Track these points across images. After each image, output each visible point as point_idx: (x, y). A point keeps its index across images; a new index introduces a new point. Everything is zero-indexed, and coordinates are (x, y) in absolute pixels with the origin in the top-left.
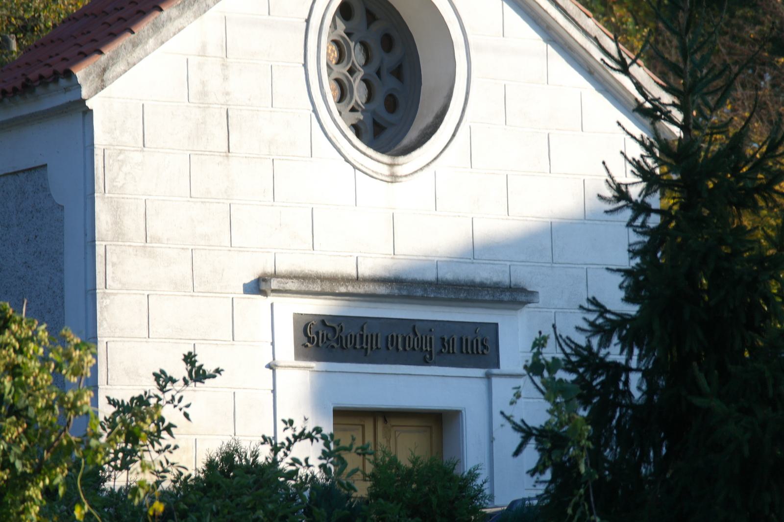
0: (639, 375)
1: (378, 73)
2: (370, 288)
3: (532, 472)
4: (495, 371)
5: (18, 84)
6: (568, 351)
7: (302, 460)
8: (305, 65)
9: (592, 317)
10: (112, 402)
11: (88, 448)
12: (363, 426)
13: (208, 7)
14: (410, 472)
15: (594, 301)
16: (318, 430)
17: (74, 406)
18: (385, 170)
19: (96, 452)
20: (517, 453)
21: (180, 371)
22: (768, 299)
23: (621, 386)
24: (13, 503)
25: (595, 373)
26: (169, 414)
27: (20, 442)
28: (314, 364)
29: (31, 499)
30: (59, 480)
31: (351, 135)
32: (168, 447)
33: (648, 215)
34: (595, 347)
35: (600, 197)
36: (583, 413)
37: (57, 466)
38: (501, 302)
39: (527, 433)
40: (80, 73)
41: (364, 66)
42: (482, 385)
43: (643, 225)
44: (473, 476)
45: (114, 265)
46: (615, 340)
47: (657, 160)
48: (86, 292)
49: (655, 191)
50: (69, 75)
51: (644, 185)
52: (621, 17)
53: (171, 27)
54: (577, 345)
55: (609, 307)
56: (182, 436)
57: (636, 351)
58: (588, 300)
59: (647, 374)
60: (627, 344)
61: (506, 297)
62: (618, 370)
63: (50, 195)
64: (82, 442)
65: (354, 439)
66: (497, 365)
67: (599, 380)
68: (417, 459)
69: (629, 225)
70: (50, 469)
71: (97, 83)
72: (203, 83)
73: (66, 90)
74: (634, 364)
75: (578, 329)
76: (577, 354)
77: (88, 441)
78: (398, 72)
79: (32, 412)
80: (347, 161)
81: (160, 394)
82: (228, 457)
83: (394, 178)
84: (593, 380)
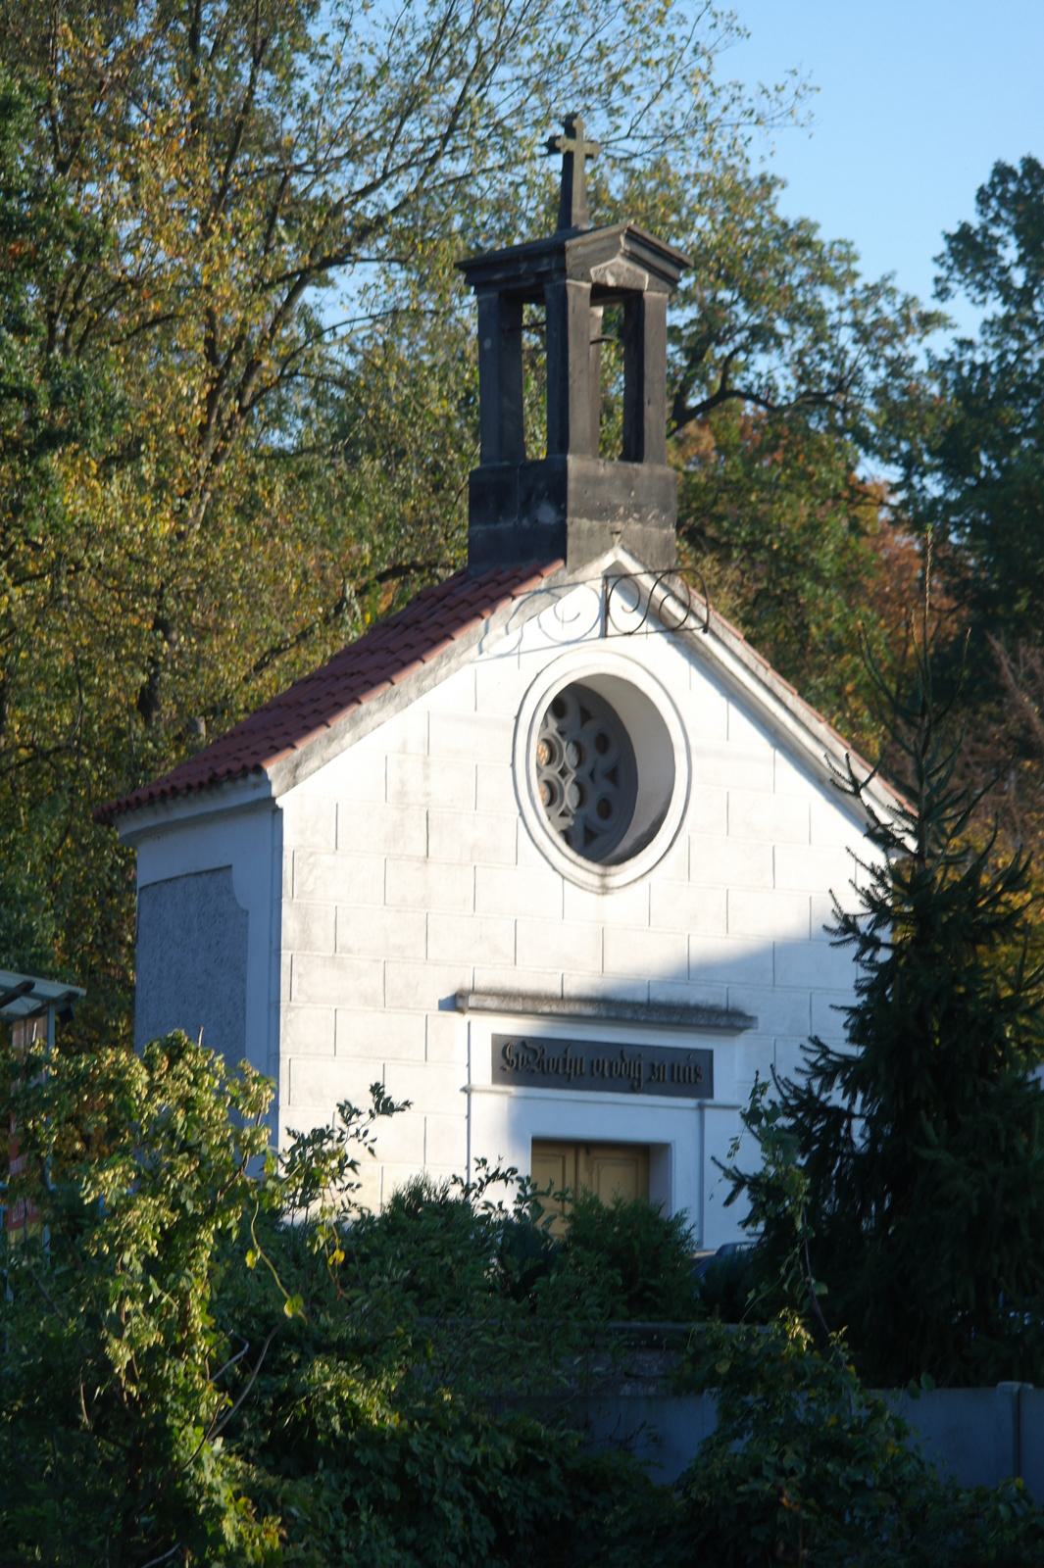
0: (862, 1122)
1: (592, 775)
2: (575, 1008)
3: (745, 1224)
4: (708, 1101)
5: (205, 778)
6: (786, 1093)
7: (496, 1205)
8: (513, 765)
9: (813, 1058)
10: (291, 1133)
11: (265, 1190)
12: (564, 1158)
13: (411, 701)
14: (611, 1215)
15: (815, 1041)
16: (513, 1171)
17: (250, 1144)
18: (595, 881)
19: (273, 1195)
20: (728, 1202)
21: (366, 1102)
22: (1003, 1043)
23: (843, 1133)
24: (183, 1247)
25: (815, 1119)
26: (353, 1149)
27: (192, 1181)
28: (512, 1089)
29: (202, 1242)
30: (232, 1223)
31: (560, 842)
32: (350, 1185)
33: (877, 949)
34: (816, 1090)
35: (826, 928)
36: (802, 1162)
37: (230, 1208)
38: (717, 1027)
39: (740, 1181)
40: (271, 769)
41: (576, 768)
42: (694, 1116)
43: (871, 959)
44: (680, 1220)
45: (300, 975)
46: (838, 1083)
47: (888, 890)
48: (270, 1005)
49: (886, 923)
50: (259, 770)
51: (873, 916)
52: (857, 710)
53: (369, 722)
54: (796, 1088)
55: (832, 1047)
56: (368, 1169)
57: (860, 1097)
58: (810, 1039)
59: (870, 1121)
60: (850, 1088)
61: (723, 1021)
62: (840, 1116)
63: (234, 899)
64: (257, 1184)
65: (552, 1183)
66: (711, 1095)
67: (819, 1126)
68: (620, 1200)
69: (856, 959)
70: (224, 1212)
71: (289, 779)
72: (403, 783)
73: (256, 786)
74: (857, 1109)
75: (798, 1070)
76: (796, 1097)
77: (265, 1183)
78: (612, 775)
79: (205, 1149)
80: (554, 869)
81: (344, 1126)
82: (416, 1192)
83: (605, 890)
84: (812, 1126)
